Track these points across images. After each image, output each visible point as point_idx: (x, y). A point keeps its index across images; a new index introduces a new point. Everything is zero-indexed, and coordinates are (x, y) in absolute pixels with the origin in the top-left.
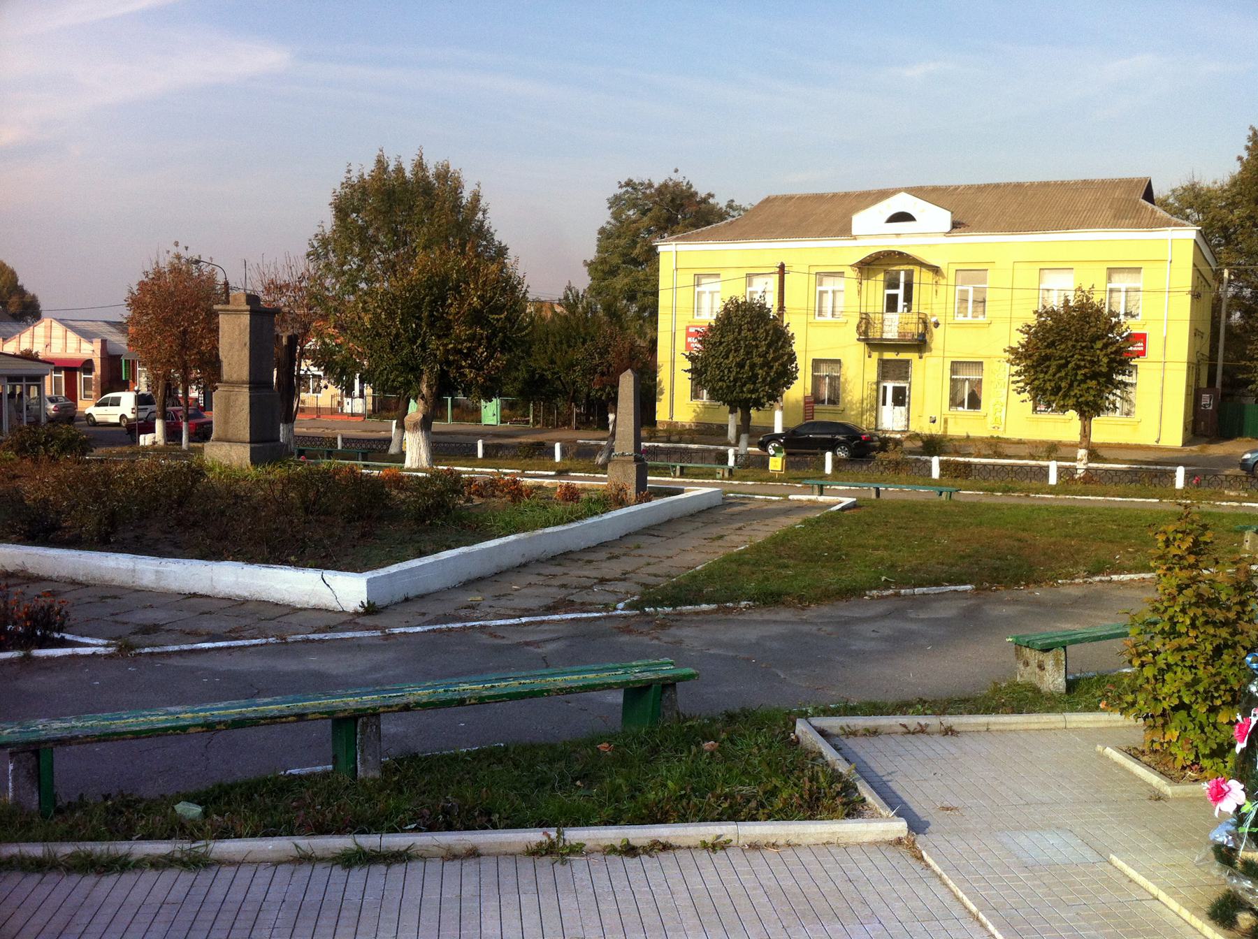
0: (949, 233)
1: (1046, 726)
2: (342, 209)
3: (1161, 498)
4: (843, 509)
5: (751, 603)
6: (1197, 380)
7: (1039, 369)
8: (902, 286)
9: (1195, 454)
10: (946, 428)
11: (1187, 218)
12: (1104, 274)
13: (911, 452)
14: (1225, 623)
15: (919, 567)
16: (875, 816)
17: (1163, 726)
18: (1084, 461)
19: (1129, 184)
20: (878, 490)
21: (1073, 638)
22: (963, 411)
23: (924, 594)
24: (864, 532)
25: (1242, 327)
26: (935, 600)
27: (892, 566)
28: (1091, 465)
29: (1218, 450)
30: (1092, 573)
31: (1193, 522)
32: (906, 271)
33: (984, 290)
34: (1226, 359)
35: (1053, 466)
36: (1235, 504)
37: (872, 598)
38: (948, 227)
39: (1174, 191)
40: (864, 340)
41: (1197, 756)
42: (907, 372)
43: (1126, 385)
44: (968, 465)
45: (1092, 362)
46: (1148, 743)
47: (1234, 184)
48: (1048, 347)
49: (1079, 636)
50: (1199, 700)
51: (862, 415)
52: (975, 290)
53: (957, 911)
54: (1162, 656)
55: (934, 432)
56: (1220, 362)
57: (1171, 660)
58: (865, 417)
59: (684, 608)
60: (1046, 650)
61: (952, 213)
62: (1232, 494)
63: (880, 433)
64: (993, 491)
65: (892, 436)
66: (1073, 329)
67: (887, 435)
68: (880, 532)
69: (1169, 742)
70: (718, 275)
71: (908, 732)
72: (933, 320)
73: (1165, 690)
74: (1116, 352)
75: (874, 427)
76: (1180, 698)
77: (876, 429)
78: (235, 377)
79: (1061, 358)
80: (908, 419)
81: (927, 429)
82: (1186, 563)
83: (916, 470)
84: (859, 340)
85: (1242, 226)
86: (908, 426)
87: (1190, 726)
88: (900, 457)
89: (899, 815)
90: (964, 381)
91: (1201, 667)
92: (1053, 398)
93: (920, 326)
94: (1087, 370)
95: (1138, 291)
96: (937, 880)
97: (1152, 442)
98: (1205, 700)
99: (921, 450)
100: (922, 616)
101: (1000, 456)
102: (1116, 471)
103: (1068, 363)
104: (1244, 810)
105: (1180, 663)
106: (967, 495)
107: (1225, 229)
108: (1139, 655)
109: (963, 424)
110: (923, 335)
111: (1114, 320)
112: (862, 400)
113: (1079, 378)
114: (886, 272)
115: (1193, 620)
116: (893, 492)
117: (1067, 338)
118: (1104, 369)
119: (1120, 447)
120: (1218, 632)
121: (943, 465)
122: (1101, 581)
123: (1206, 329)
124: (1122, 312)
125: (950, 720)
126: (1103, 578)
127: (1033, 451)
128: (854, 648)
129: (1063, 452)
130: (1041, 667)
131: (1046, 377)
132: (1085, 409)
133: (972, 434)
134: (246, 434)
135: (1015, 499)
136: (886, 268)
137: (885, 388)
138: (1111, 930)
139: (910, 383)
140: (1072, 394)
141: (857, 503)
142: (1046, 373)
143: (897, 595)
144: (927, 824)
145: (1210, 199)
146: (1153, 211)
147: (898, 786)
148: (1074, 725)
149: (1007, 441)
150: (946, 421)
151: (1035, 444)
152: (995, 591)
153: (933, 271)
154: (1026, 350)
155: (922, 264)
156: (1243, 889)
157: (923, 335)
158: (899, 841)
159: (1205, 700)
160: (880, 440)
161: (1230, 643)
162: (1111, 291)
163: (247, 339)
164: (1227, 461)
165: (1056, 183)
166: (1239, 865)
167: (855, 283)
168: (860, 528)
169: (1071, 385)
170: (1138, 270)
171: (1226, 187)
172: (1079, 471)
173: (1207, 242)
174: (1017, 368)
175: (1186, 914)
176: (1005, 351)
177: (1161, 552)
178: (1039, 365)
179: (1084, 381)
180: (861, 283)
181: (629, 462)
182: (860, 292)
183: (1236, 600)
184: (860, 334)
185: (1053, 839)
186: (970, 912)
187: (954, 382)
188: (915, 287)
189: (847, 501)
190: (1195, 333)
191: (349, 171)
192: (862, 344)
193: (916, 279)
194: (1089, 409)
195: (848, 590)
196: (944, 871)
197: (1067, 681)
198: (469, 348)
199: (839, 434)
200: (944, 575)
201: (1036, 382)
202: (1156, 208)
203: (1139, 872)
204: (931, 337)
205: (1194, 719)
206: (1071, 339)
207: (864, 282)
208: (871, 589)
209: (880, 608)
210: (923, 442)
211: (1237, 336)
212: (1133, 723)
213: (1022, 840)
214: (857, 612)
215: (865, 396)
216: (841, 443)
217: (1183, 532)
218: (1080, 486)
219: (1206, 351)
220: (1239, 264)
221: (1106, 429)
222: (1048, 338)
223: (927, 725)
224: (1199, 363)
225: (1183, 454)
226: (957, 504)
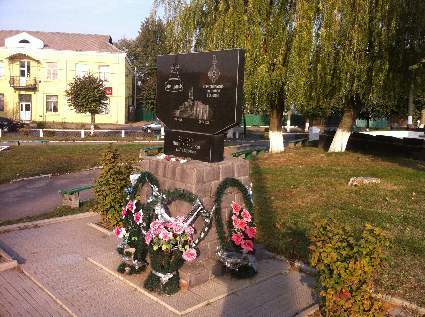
0: (43, 49)
1: (71, 219)
3: (117, 141)
4: (4, 150)
6: (129, 103)
7: (76, 98)
8: (26, 67)
9: (128, 126)
10: (45, 119)
11: (123, 50)
12: (97, 67)
13: (33, 128)
14: (124, 179)
15: (32, 169)
16: (6, 261)
17: (106, 214)
18: (93, 129)
19: (104, 37)
20: (19, 142)
21: (81, 189)
22: (52, 113)
23: (33, 179)
24: (11, 158)
25: (142, 86)
26: (37, 181)
27: (22, 170)
28: (95, 131)
29: (135, 125)
30: (92, 167)
31: (113, 149)
32: (27, 62)
33: (56, 70)
34: (137, 96)
35: (82, 131)
36: (140, 141)
37: (13, 182)
38: (42, 47)
39: (119, 41)
40: (12, 87)
41: (117, 221)
42: (30, 99)
43: (105, 103)
44: (53, 132)
45: (93, 96)
46: (102, 220)
47: (137, 40)
48: (79, 91)
49: (83, 188)
50: (117, 204)
51: (14, 114)
52: (53, 70)
53: (35, 288)
54: (105, 192)
55: (41, 120)
56: (135, 97)
57: (107, 193)
58: (15, 115)
60: (72, 194)
61: (44, 41)
62: (139, 138)
63: (20, 121)
64: (62, 140)
65: (25, 122)
66: (87, 85)
67: (23, 122)
68: (18, 158)
69: (109, 219)
70: (108, 66)
71: (21, 229)
72: (39, 80)
73: (106, 202)
74: (101, 93)
75: (18, 119)
76: (111, 204)
77: (19, 120)
79: (83, 95)
80: (31, 116)
81: (38, 119)
82: (111, 162)
83: (34, 134)
84: (10, 86)
85: (140, 54)
86: (31, 118)
87: (115, 212)
88: (28, 130)
89: (14, 259)
90: (51, 102)
91: (117, 194)
92: (81, 108)
93: (34, 82)
94: (92, 99)
95: (108, 73)
96: (28, 279)
97: (115, 123)
98: (118, 204)
99: (37, 127)
100: (32, 187)
101: (65, 128)
102: (103, 132)
103: (86, 96)
104: (126, 236)
105: (110, 193)
106: (53, 142)
107: (135, 54)
108: (97, 192)
109: (51, 118)
110: (35, 85)
111: (101, 83)
112: (13, 109)
113: (90, 101)
114: (20, 62)
115: (114, 179)
116: (25, 143)
117: (85, 88)
118: (98, 98)
119: (106, 124)
120: (121, 182)
121: (44, 132)
122: (95, 169)
123: (130, 86)
124: (104, 80)
125: (36, 223)
126: (96, 168)
127: (77, 126)
128: (5, 201)
129: (86, 126)
130: (71, 200)
131: (79, 101)
132: (92, 112)
133: (55, 121)
135: (70, 143)
136: (20, 60)
137: (22, 105)
138: (87, 282)
139: (31, 103)
140: (88, 107)
141: (10, 148)
142: (79, 100)
143: (23, 180)
144: (26, 260)
145: (130, 44)
146: (112, 47)
147: (16, 249)
148: (80, 217)
149: (68, 123)
150: (45, 117)
151: (77, 124)
152: (59, 175)
153: (38, 62)
154: (71, 92)
155: (33, 59)
156: (126, 260)
157: (35, 85)
158: (15, 268)
159: (118, 204)
160: (21, 124)
161: (125, 185)
162: (100, 72)
164: (138, 128)
165: (80, 34)
166: (125, 254)
167: (8, 65)
168: (10, 157)
169: (87, 104)
170: (108, 66)
171: (135, 41)
172: (91, 133)
173: (130, 58)
174: (68, 98)
175: (111, 272)
176: (64, 92)
177: (103, 159)
178: (76, 97)
179: (91, 103)
180: (10, 65)
182: (10, 68)
183: (127, 172)
184: (11, 84)
185: (70, 256)
186: (39, 287)
187: (48, 103)
188: (31, 68)
189: (6, 147)
190: (127, 88)
192: (12, 88)
193: (31, 65)
194: (94, 112)
195: (4, 180)
196: (31, 275)
197: (80, 203)
199: (4, 122)
200: (40, 172)
201: (75, 103)
202: (113, 46)
203: (97, 262)
204: (38, 86)
205: (116, 210)
206: (86, 88)
207: (11, 65)
208: (12, 179)
209: (16, 186)
210: (37, 124)
211: (140, 89)
212: (98, 214)
213: (59, 259)
214: (6, 188)
215: (14, 108)
216: (5, 125)
217: (110, 152)
218: (92, 138)
219: (131, 93)
220: (140, 66)
221: (99, 119)
222: (79, 88)
223: (28, 226)
224: (129, 98)
225: (125, 126)
226: (48, 146)
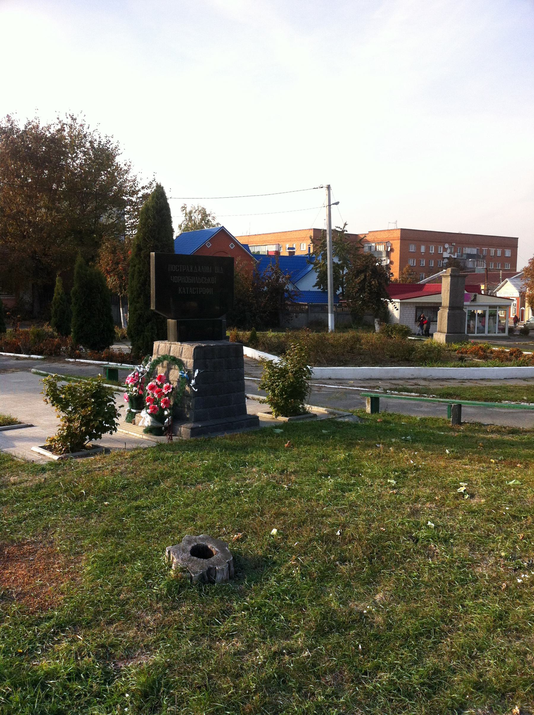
134: (446, 330)
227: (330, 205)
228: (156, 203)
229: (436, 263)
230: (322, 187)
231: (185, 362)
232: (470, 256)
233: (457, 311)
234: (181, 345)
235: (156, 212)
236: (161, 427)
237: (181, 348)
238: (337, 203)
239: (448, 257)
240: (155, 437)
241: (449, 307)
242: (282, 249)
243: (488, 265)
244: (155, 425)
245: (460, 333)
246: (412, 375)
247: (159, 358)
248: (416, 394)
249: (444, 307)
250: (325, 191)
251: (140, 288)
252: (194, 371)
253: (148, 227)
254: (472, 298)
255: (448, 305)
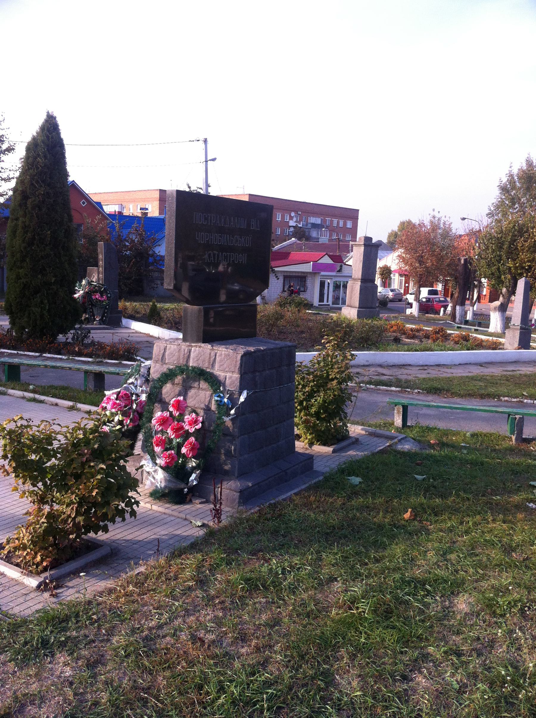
2: (504, 189)
5: (421, 391)
59: (381, 387)
78: (356, 277)
134: (357, 304)
163: (362, 259)
181: (517, 329)
191: (511, 167)
198: (529, 266)
227: (206, 161)
228: (48, 137)
229: (283, 231)
230: (198, 141)
231: (222, 378)
232: (314, 226)
233: (369, 285)
234: (213, 349)
235: (48, 150)
236: (182, 490)
237: (213, 354)
238: (214, 160)
239: (295, 225)
240: (175, 507)
241: (362, 279)
242: (125, 209)
243: (331, 235)
244: (172, 485)
245: (372, 308)
246: (367, 361)
247: (170, 370)
248: (398, 389)
249: (355, 280)
250: (202, 144)
251: (25, 248)
252: (240, 394)
253: (38, 168)
254: (338, 268)
255: (360, 277)
